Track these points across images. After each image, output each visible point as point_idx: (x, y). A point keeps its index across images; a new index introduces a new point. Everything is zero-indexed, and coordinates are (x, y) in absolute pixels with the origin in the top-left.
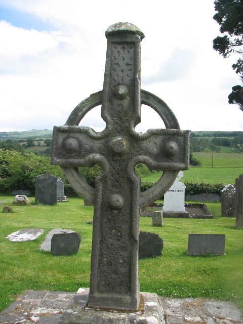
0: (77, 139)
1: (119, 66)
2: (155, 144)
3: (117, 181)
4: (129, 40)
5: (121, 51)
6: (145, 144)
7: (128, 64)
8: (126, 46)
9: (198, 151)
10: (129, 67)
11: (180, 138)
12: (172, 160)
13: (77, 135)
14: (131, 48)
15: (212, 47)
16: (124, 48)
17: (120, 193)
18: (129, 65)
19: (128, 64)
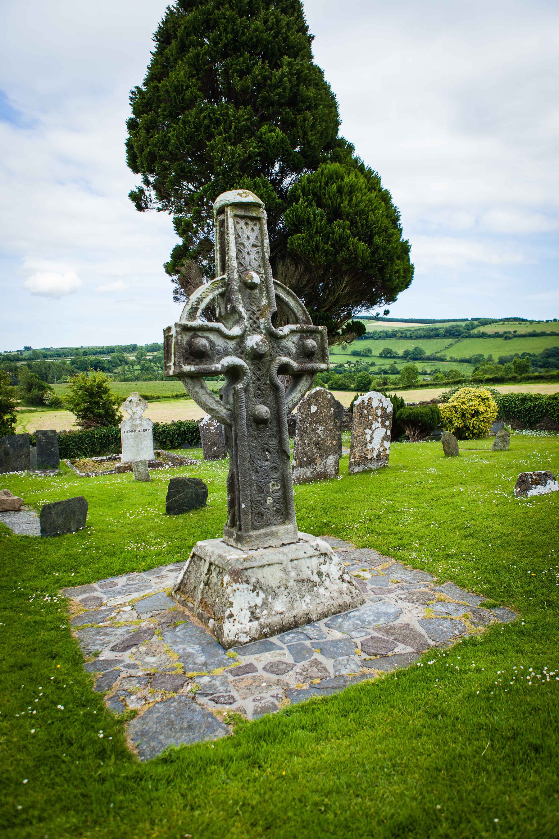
0: (207, 338)
1: (244, 246)
2: (293, 343)
3: (259, 389)
4: (254, 215)
5: (244, 228)
6: (284, 342)
7: (253, 246)
8: (249, 222)
9: (465, 438)
10: (256, 249)
11: (318, 335)
12: (312, 360)
13: (206, 334)
14: (255, 224)
15: (137, 211)
16: (246, 224)
17: (264, 403)
18: (256, 246)
19: (253, 246)
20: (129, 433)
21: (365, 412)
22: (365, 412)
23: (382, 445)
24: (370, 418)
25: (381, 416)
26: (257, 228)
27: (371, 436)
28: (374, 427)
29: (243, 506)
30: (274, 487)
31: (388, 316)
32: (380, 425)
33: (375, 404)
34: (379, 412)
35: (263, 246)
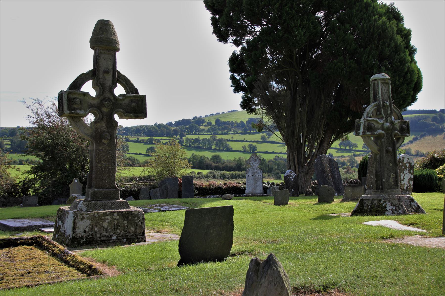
20: (251, 177)
21: (401, 164)
22: (401, 164)
23: (409, 183)
24: (403, 167)
25: (409, 167)
26: (387, 86)
27: (403, 177)
28: (405, 172)
29: (384, 180)
30: (392, 175)
31: (233, 139)
32: (408, 172)
33: (406, 161)
34: (408, 165)
35: (389, 93)
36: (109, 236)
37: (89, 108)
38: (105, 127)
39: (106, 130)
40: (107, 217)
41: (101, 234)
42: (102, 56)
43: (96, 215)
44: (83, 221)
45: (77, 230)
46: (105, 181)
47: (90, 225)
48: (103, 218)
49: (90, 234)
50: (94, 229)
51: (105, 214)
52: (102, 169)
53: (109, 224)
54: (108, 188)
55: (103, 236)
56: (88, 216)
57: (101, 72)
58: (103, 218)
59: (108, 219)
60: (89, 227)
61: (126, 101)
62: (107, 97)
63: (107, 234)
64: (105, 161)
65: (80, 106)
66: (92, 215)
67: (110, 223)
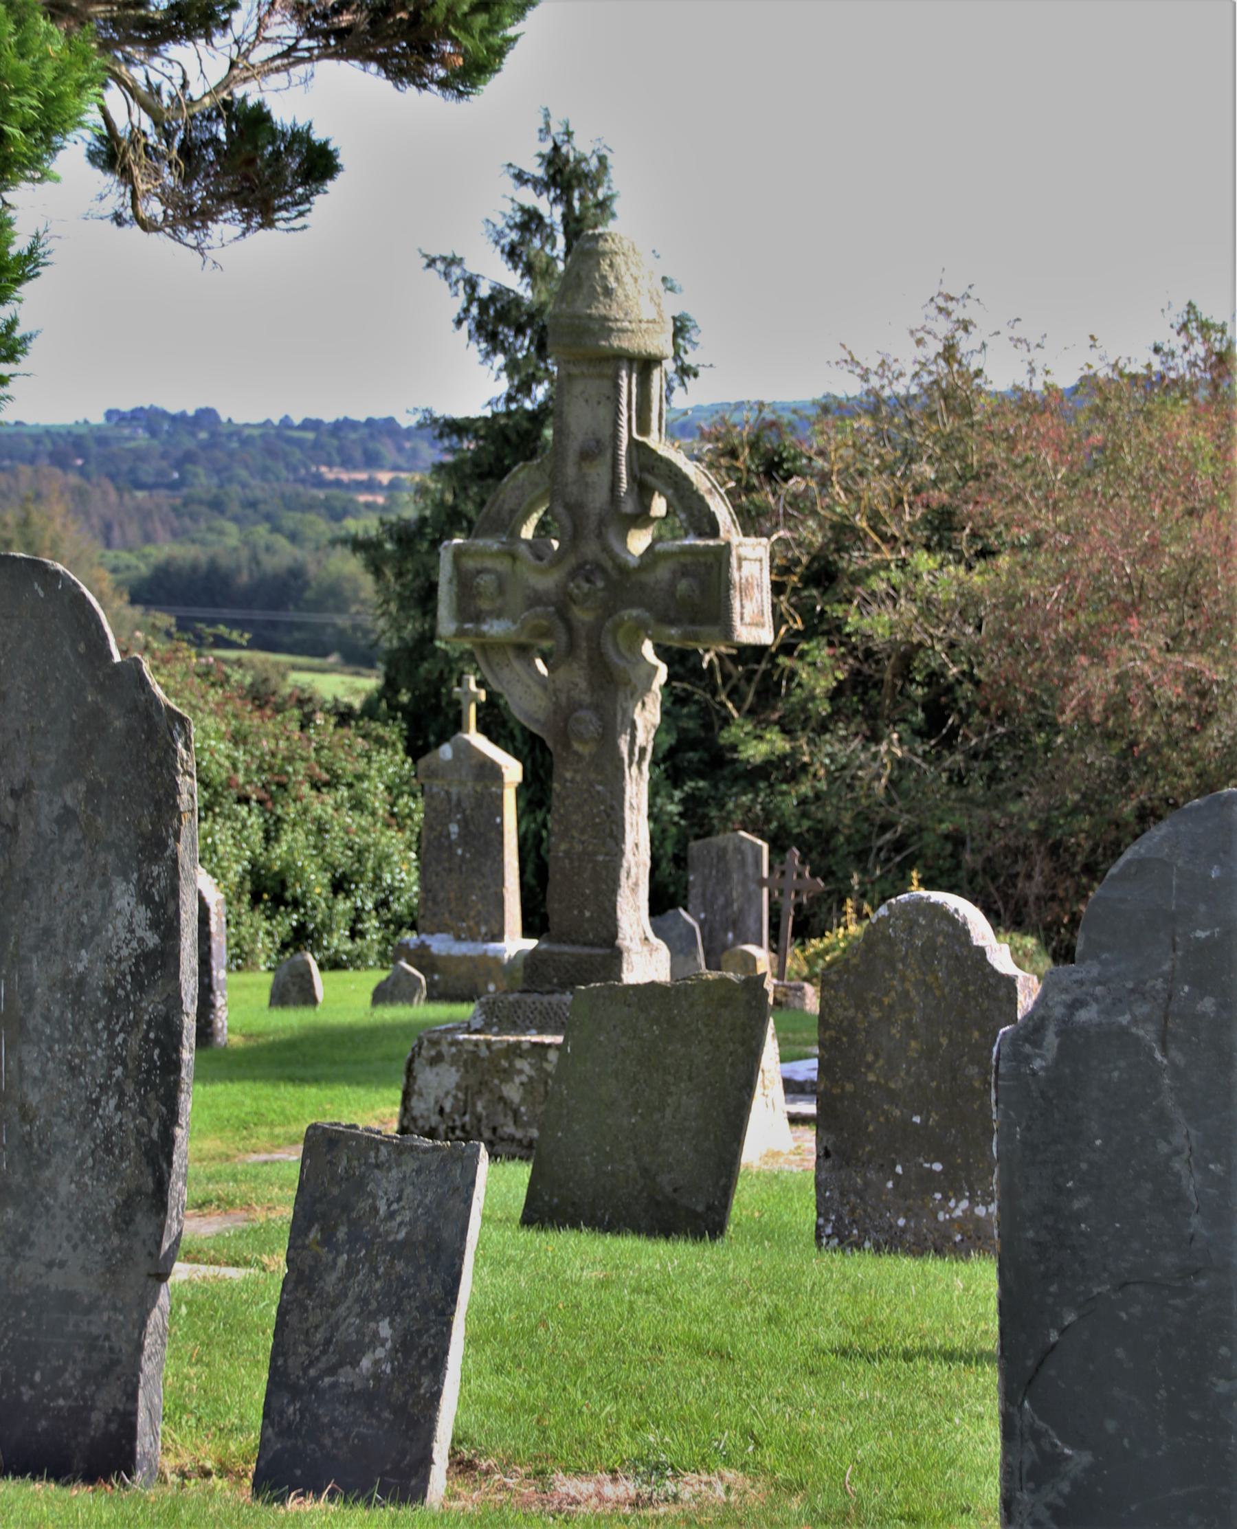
36: (525, 1142)
37: (530, 606)
38: (583, 685)
39: (587, 699)
40: (520, 1064)
41: (494, 1130)
42: (578, 387)
43: (484, 1052)
44: (435, 1070)
45: (414, 1102)
46: (581, 912)
47: (458, 1087)
48: (504, 1063)
49: (458, 1123)
50: (474, 1105)
51: (514, 1050)
52: (572, 861)
53: (525, 1091)
54: (592, 944)
55: (502, 1139)
56: (454, 1050)
57: (572, 456)
58: (504, 1063)
59: (521, 1072)
60: (455, 1097)
61: (663, 572)
62: (590, 557)
63: (519, 1134)
64: (583, 832)
65: (499, 602)
66: (471, 1048)
67: (528, 1087)
